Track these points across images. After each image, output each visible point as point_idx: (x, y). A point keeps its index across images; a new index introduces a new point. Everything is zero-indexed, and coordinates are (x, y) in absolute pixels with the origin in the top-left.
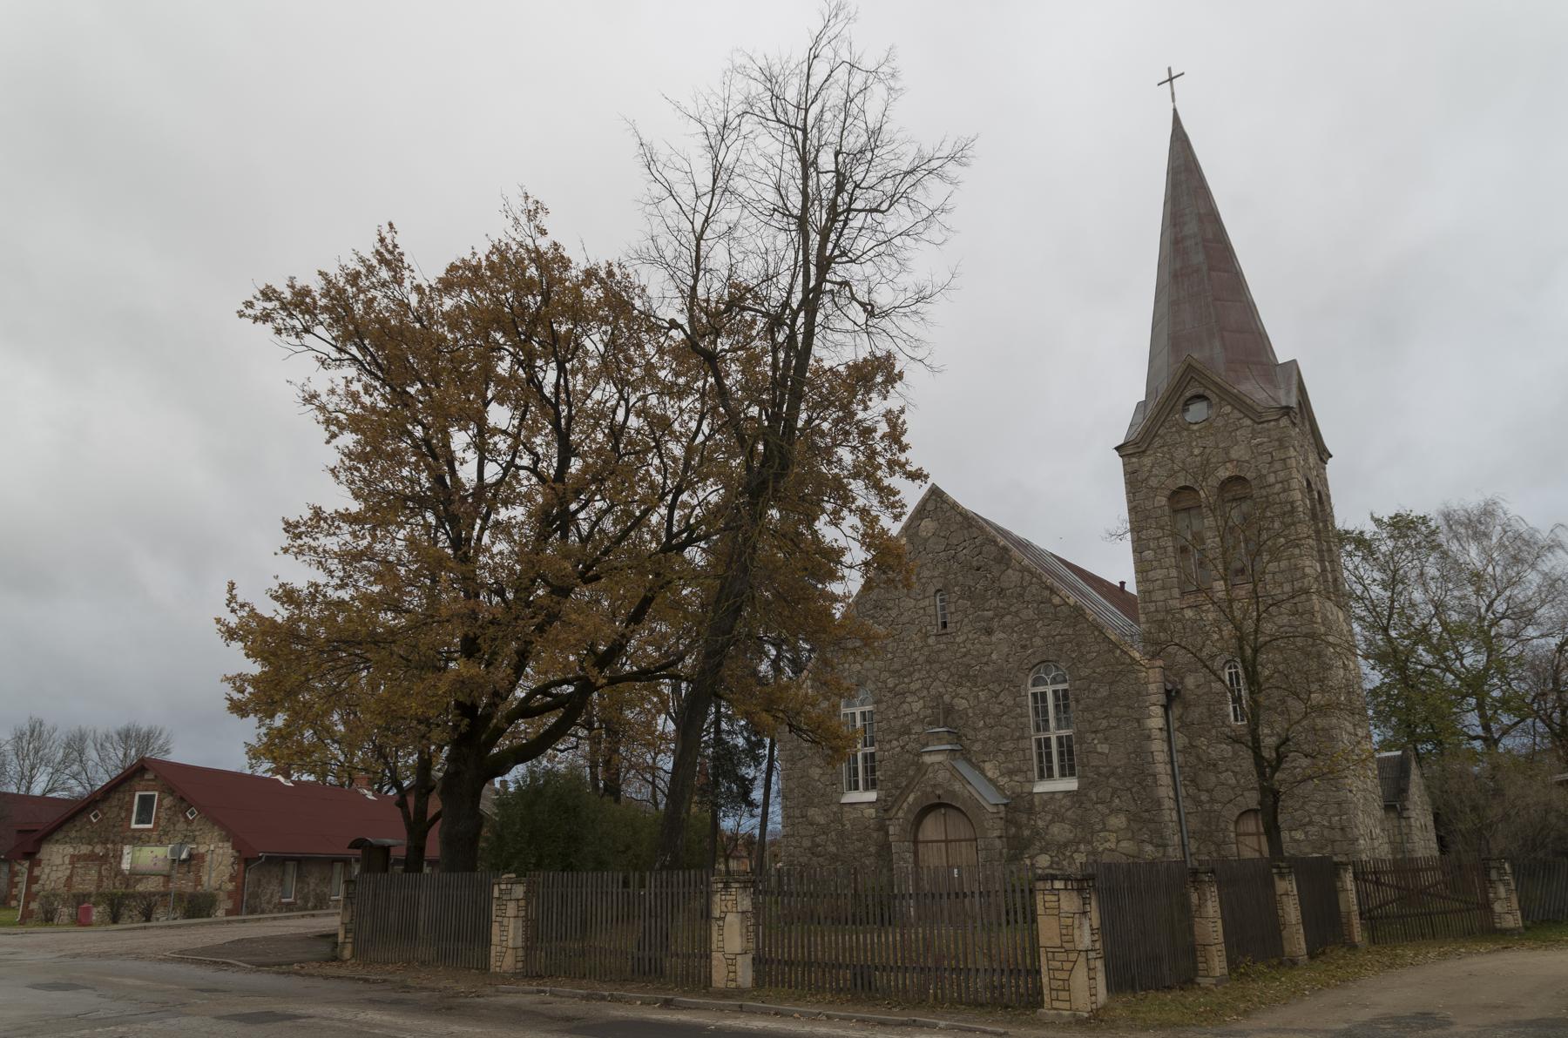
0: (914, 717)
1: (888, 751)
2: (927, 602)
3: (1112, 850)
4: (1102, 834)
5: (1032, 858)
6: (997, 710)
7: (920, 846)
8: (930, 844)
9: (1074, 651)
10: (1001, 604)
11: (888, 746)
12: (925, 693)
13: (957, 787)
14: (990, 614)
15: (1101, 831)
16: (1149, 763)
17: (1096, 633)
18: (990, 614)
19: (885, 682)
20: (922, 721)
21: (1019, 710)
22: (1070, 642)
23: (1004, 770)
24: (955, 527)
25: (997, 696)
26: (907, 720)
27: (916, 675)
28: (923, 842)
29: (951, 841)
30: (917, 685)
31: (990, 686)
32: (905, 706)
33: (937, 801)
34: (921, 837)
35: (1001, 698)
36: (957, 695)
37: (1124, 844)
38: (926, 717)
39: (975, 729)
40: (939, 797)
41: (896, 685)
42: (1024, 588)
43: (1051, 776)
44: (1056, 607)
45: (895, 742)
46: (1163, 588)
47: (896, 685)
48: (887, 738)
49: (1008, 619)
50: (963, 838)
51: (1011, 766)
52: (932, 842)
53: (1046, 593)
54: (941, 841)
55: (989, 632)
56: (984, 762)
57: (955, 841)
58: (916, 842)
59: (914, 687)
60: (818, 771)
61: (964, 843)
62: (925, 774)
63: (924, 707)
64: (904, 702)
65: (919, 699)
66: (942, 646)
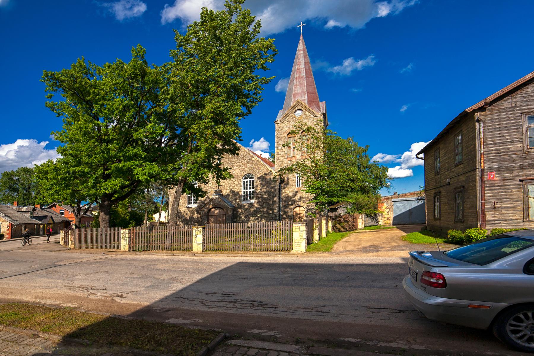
0: (209, 187)
6: (234, 185)
7: (209, 217)
13: (221, 203)
14: (234, 162)
18: (234, 162)
20: (212, 188)
34: (210, 215)
35: (235, 182)
42: (244, 156)
43: (191, 203)
49: (239, 164)
53: (251, 157)
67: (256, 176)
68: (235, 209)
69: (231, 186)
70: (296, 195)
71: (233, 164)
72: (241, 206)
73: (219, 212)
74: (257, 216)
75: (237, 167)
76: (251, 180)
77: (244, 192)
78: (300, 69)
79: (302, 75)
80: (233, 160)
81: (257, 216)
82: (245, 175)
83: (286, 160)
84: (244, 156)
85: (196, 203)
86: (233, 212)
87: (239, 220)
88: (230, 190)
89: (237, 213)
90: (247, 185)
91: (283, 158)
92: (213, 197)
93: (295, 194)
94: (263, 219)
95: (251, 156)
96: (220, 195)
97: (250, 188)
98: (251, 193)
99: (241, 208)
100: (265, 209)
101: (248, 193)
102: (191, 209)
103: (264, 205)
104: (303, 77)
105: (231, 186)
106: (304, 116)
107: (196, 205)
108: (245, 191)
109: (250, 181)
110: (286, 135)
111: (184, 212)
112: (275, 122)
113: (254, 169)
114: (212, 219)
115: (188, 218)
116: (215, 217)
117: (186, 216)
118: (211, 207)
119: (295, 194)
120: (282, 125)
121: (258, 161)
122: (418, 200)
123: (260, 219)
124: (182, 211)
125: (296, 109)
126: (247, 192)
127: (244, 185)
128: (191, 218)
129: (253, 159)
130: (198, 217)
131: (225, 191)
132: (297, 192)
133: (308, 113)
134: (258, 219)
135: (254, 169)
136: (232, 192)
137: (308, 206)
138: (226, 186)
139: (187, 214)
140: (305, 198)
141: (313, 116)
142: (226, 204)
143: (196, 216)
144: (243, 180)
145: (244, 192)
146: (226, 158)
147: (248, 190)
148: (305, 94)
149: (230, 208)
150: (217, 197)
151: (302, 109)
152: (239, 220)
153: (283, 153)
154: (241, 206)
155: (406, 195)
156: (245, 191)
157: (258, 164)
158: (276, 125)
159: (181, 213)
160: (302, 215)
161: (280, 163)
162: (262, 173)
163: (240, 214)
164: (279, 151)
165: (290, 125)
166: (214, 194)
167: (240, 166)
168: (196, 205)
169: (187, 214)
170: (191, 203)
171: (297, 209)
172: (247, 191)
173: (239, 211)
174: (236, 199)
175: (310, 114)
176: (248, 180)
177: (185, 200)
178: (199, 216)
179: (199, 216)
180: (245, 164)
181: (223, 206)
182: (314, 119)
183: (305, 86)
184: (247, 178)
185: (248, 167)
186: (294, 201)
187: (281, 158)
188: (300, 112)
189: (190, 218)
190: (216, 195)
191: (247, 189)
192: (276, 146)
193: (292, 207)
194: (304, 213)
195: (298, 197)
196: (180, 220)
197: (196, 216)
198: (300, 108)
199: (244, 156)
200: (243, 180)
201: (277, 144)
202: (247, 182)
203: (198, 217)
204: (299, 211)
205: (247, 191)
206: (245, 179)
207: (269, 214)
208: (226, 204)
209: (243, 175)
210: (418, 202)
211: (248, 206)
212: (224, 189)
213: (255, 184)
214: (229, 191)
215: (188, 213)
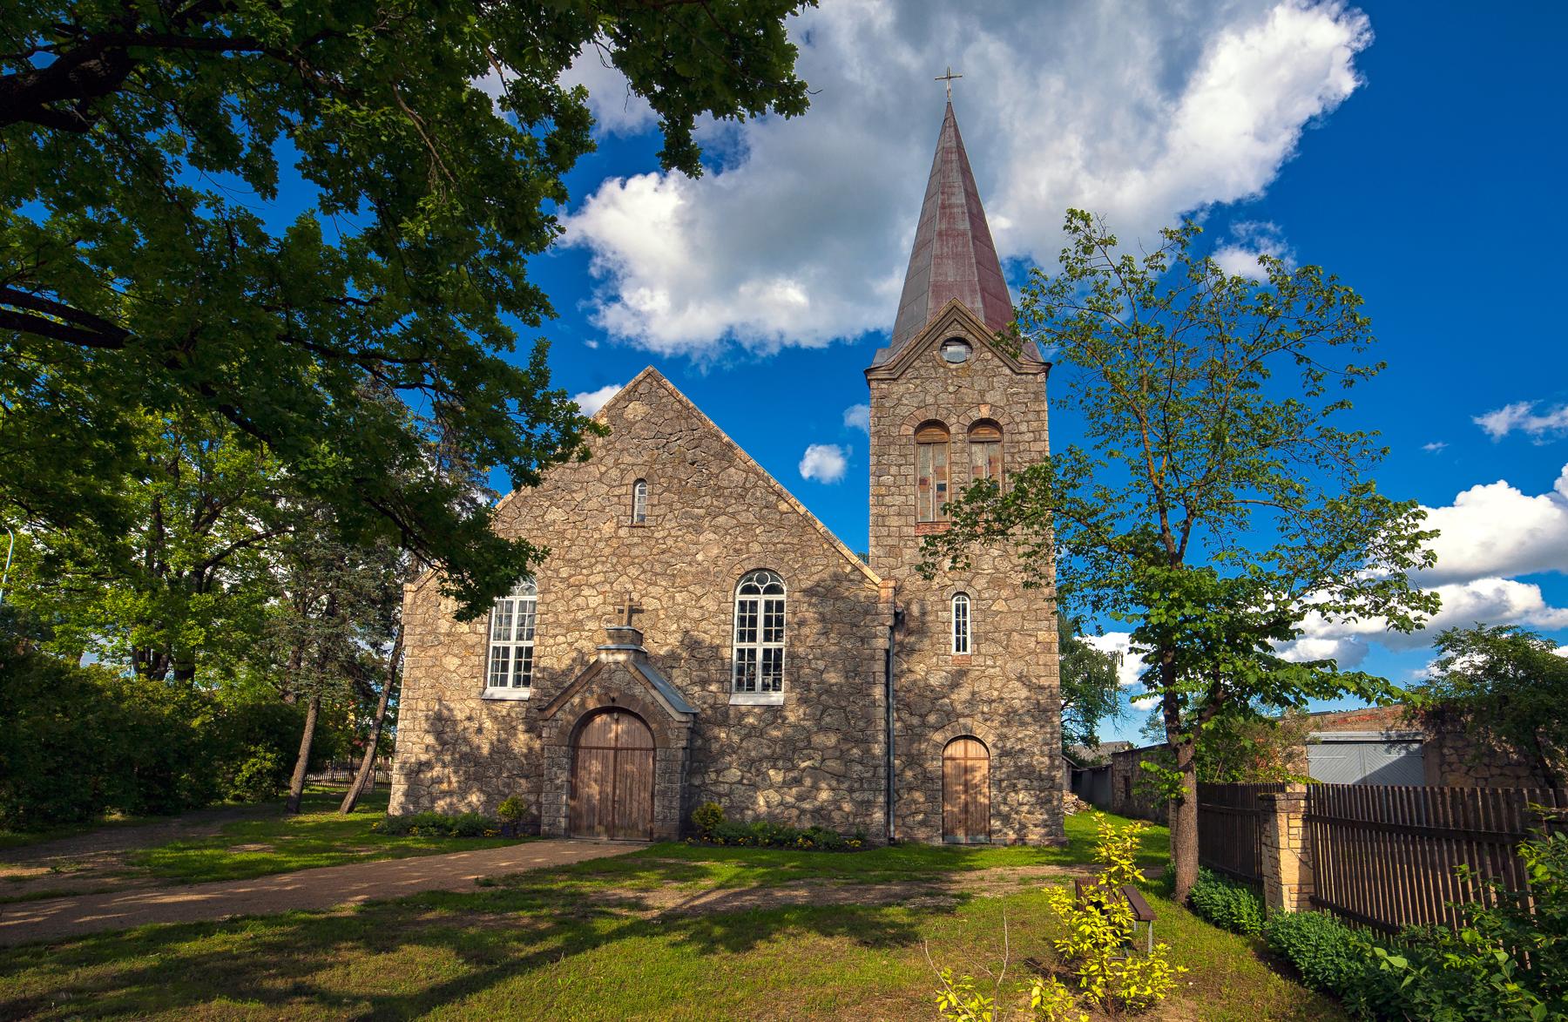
0: (589, 613)
1: (552, 646)
2: (624, 490)
3: (815, 768)
4: (805, 752)
5: (718, 772)
6: (696, 614)
7: (581, 753)
8: (594, 751)
9: (797, 562)
10: (715, 503)
11: (551, 641)
12: (607, 587)
13: (638, 690)
14: (702, 511)
15: (805, 748)
16: (869, 683)
17: (825, 546)
18: (702, 511)
19: (557, 571)
20: (599, 618)
21: (723, 617)
22: (794, 552)
23: (697, 679)
24: (672, 414)
25: (699, 598)
26: (580, 616)
27: (599, 567)
28: (585, 748)
29: (622, 749)
30: (600, 578)
31: (691, 588)
32: (580, 600)
33: (611, 704)
34: (583, 742)
35: (703, 602)
36: (646, 595)
37: (828, 763)
38: (604, 614)
39: (665, 632)
40: (613, 700)
41: (570, 577)
42: (746, 490)
43: (504, 683)
44: (782, 513)
45: (561, 639)
46: (899, 515)
47: (570, 577)
48: (552, 632)
49: (721, 519)
50: (637, 746)
51: (705, 675)
52: (597, 748)
53: (773, 498)
54: (610, 748)
55: (698, 530)
56: (672, 667)
57: (627, 749)
58: (575, 746)
59: (592, 580)
60: (457, 661)
61: (637, 752)
62: (597, 674)
63: (604, 603)
64: (579, 595)
65: (599, 593)
66: (636, 540)
67: (796, 584)
68: (698, 726)
69: (683, 616)
70: (954, 685)
71: (698, 517)
72: (726, 715)
73: (628, 732)
74: (794, 767)
75: (712, 536)
76: (775, 598)
77: (741, 651)
78: (950, 206)
79: (961, 227)
80: (699, 502)
81: (794, 767)
82: (747, 574)
83: (911, 531)
84: (746, 490)
85: (527, 682)
86: (691, 741)
87: (716, 783)
88: (679, 636)
89: (705, 750)
90: (768, 621)
91: (902, 521)
92: (603, 656)
93: (955, 683)
94: (823, 785)
95: (775, 492)
96: (637, 651)
97: (767, 638)
98: (773, 661)
99: (729, 726)
100: (832, 740)
101: (760, 656)
102: (502, 710)
103: (828, 719)
104: (964, 234)
105: (683, 616)
106: (978, 366)
107: (525, 693)
108: (746, 645)
109: (768, 604)
110: (911, 431)
111: (470, 719)
112: (868, 372)
113: (785, 551)
114: (596, 766)
115: (486, 750)
116: (605, 758)
117: (476, 740)
118: (592, 704)
119: (955, 683)
120: (898, 389)
121: (804, 516)
122: (1391, 743)
123: (808, 782)
124: (459, 716)
125: (949, 334)
126: (752, 652)
127: (742, 619)
128: (501, 750)
129: (784, 507)
130: (530, 749)
131: (659, 637)
132: (962, 673)
133: (989, 355)
134: (797, 781)
135: (785, 551)
136: (692, 645)
137: (1003, 737)
138: (662, 614)
139: (480, 730)
140: (991, 702)
141: (1008, 371)
142: (661, 700)
143: (521, 741)
144: (740, 598)
145: (741, 651)
146: (667, 490)
147: (760, 646)
148: (973, 291)
149: (677, 717)
150: (621, 657)
151: (970, 337)
152: (716, 783)
153: (899, 500)
154: (723, 716)
155: (1345, 720)
156: (746, 645)
157: (804, 533)
158: (874, 384)
159: (455, 722)
160: (978, 776)
161: (890, 541)
162: (819, 571)
163: (722, 753)
164: (883, 491)
165: (926, 392)
166: (609, 644)
167: (727, 533)
168: (525, 693)
169: (480, 730)
170: (504, 683)
171: (956, 750)
172: (751, 645)
173: (717, 738)
174: (704, 683)
175: (997, 362)
176: (761, 599)
177: (475, 660)
178: (537, 744)
179: (537, 744)
180: (747, 527)
181: (645, 707)
182: (1012, 383)
183: (971, 265)
184: (756, 591)
185: (761, 539)
186: (950, 715)
187: (894, 521)
188: (962, 349)
189: (494, 750)
190: (619, 650)
191: (753, 638)
192: (872, 469)
193: (938, 737)
194: (983, 769)
195: (962, 694)
196: (447, 758)
197: (521, 741)
198: (963, 334)
199: (743, 487)
200: (740, 598)
201: (879, 462)
202: (754, 604)
203: (530, 749)
204: (966, 758)
205: (751, 645)
206: (748, 590)
207: (848, 762)
208: (661, 700)
209: (738, 571)
210: (1388, 751)
211: (759, 717)
212: (653, 627)
213: (787, 616)
214: (674, 640)
215: (488, 724)
